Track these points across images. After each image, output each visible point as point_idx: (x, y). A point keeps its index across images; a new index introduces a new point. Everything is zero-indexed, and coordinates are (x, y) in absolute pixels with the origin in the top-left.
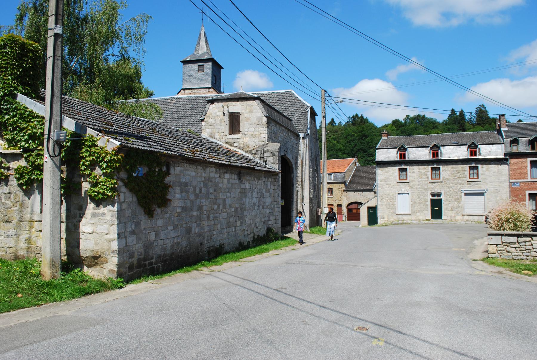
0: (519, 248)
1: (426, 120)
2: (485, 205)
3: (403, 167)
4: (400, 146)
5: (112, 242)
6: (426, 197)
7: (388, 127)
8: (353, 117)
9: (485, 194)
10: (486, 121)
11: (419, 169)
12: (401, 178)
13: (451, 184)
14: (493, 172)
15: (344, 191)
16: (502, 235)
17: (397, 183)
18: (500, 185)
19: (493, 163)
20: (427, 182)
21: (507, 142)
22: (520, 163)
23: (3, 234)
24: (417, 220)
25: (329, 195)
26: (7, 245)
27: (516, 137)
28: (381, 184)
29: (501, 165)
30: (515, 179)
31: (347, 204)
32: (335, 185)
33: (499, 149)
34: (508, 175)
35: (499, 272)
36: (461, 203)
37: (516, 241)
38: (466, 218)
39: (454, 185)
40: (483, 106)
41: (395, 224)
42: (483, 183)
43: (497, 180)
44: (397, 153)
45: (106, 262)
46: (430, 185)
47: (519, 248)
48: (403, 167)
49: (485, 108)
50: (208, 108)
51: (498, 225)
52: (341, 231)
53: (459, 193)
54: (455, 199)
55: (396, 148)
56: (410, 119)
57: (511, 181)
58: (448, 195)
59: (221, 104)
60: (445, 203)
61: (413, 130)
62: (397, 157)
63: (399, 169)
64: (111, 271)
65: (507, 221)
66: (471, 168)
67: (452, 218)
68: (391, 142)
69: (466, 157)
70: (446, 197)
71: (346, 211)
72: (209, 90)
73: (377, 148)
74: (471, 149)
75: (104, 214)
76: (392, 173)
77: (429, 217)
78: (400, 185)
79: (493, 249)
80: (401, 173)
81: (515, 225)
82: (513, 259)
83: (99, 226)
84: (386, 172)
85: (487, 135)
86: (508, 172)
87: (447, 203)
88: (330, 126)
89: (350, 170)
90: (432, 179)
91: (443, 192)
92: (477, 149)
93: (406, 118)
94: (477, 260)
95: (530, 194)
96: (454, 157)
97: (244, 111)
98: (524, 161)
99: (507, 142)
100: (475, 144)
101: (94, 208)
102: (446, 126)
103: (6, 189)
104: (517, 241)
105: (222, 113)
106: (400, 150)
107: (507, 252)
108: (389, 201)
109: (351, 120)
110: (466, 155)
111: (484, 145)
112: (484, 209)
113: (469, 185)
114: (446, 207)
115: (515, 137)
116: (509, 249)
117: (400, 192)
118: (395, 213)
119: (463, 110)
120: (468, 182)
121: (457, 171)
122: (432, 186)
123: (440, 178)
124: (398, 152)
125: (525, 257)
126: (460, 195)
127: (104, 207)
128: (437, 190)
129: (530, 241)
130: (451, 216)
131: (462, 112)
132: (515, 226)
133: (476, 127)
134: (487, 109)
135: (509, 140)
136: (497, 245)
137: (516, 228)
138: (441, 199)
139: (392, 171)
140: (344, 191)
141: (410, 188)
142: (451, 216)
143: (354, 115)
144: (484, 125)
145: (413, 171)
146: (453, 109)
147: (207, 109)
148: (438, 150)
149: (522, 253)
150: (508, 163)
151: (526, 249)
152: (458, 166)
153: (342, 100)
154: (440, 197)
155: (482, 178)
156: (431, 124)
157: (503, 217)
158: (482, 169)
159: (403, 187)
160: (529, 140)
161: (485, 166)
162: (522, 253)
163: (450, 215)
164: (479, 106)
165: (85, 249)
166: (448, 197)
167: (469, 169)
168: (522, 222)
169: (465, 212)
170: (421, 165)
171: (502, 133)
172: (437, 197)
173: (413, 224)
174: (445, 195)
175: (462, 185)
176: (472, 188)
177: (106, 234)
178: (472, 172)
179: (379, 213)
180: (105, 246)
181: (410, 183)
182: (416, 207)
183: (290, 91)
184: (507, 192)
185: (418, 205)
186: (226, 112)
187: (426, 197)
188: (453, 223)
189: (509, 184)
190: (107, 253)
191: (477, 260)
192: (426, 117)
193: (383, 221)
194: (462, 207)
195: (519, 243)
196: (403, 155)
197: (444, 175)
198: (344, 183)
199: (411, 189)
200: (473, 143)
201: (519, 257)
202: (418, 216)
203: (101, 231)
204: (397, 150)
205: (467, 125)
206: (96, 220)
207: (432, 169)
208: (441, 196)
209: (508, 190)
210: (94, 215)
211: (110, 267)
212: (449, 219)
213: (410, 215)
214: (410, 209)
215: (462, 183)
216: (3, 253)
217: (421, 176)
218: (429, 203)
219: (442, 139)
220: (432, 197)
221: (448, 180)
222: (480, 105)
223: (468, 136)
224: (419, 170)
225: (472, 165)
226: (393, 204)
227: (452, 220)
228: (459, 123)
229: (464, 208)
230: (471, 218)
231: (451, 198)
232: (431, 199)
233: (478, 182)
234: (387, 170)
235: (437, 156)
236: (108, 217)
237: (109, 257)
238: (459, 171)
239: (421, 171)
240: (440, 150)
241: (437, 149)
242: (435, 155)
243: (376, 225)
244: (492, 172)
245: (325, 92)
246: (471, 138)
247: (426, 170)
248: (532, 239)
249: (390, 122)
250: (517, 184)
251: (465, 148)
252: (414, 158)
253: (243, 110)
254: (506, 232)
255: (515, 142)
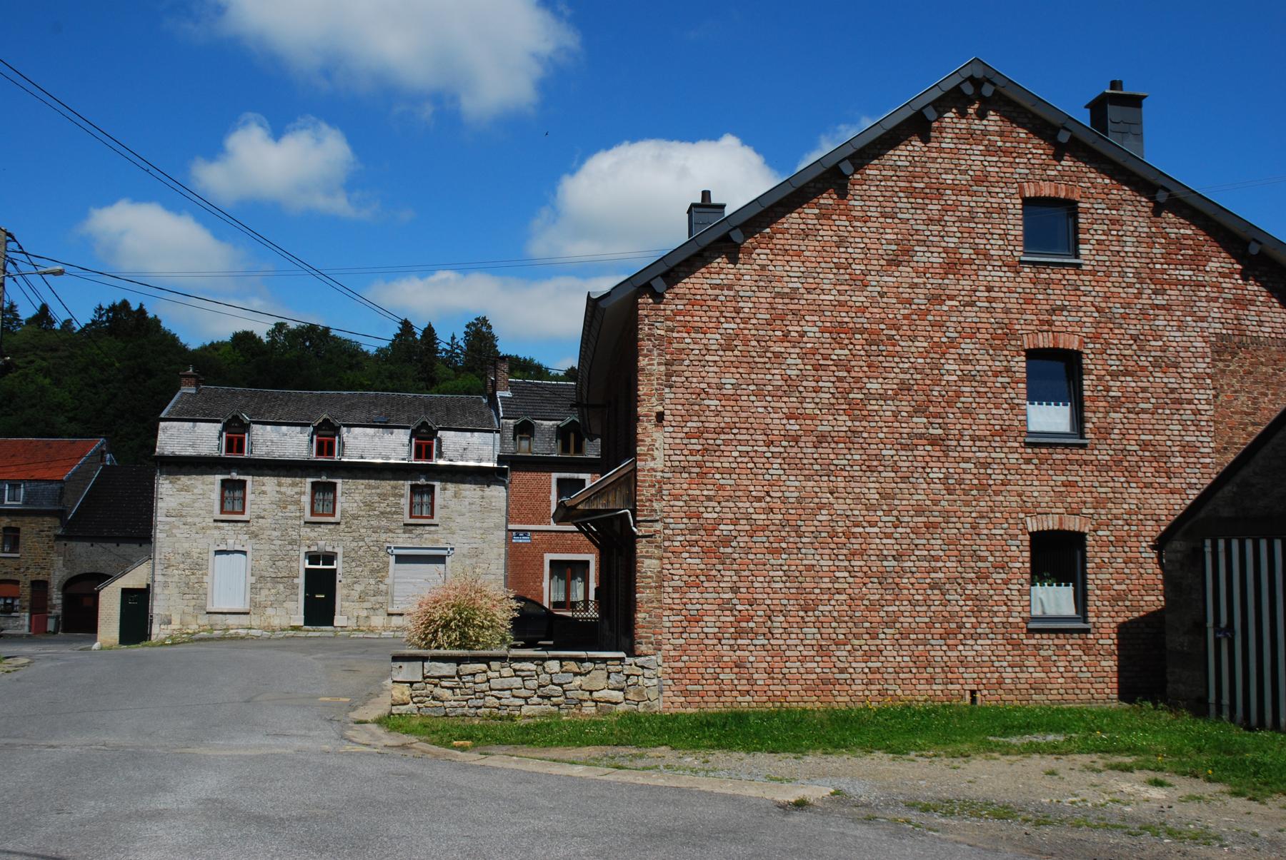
0: (460, 688)
1: (332, 343)
6: (294, 564)
7: (220, 352)
8: (113, 308)
9: (448, 559)
11: (280, 485)
13: (363, 531)
15: (58, 537)
16: (424, 659)
22: (534, 482)
24: (264, 629)
25: (7, 549)
27: (528, 418)
28: (167, 523)
29: (488, 486)
30: (521, 522)
31: (66, 579)
32: (27, 519)
33: (486, 444)
34: (504, 513)
35: (404, 747)
36: (387, 581)
37: (453, 673)
39: (370, 532)
40: (484, 321)
41: (201, 640)
42: (444, 529)
43: (478, 525)
44: (221, 435)
46: (306, 531)
47: (460, 688)
49: (490, 327)
51: (427, 635)
52: (26, 661)
54: (372, 571)
55: (218, 422)
57: (511, 527)
60: (344, 581)
62: (219, 448)
65: (446, 626)
66: (415, 490)
68: (206, 402)
69: (404, 459)
71: (59, 601)
73: (162, 415)
77: (299, 620)
78: (222, 528)
79: (403, 694)
80: (227, 494)
81: (464, 635)
82: (446, 715)
84: (186, 489)
85: (463, 405)
88: (34, 328)
89: (82, 475)
91: (339, 551)
93: (273, 331)
94: (366, 722)
95: (552, 562)
96: (373, 458)
102: (385, 367)
104: (457, 672)
107: (434, 698)
109: (104, 319)
110: (405, 455)
111: (453, 433)
113: (407, 535)
114: (345, 592)
116: (438, 691)
117: (223, 547)
118: (203, 607)
120: (405, 525)
121: (379, 495)
122: (312, 535)
123: (333, 514)
124: (224, 434)
125: (473, 711)
126: (385, 559)
128: (325, 545)
129: (485, 672)
132: (465, 637)
133: (462, 375)
134: (495, 331)
136: (412, 683)
137: (464, 642)
138: (335, 570)
139: (201, 486)
140: (58, 537)
143: (117, 304)
149: (467, 701)
150: (507, 482)
151: (475, 692)
153: (59, 267)
157: (437, 616)
158: (444, 493)
159: (231, 533)
160: (558, 426)
162: (467, 701)
163: (355, 614)
168: (482, 627)
173: (253, 638)
175: (391, 535)
178: (417, 499)
182: (265, 592)
185: (269, 585)
187: (294, 564)
188: (361, 635)
191: (366, 722)
193: (168, 632)
195: (460, 677)
196: (235, 443)
197: (346, 505)
198: (60, 514)
199: (253, 541)
200: (424, 424)
201: (459, 711)
204: (219, 426)
205: (441, 369)
207: (315, 486)
212: (352, 624)
213: (248, 613)
217: (282, 504)
218: (301, 581)
219: (347, 406)
221: (355, 517)
223: (417, 403)
224: (278, 489)
226: (200, 582)
229: (392, 597)
231: (360, 569)
233: (433, 528)
234: (189, 483)
239: (283, 489)
241: (332, 433)
242: (325, 447)
243: (144, 643)
245: (8, 238)
246: (423, 409)
247: (297, 489)
248: (489, 667)
249: (227, 338)
251: (402, 436)
252: (267, 454)
254: (442, 652)
255: (525, 430)
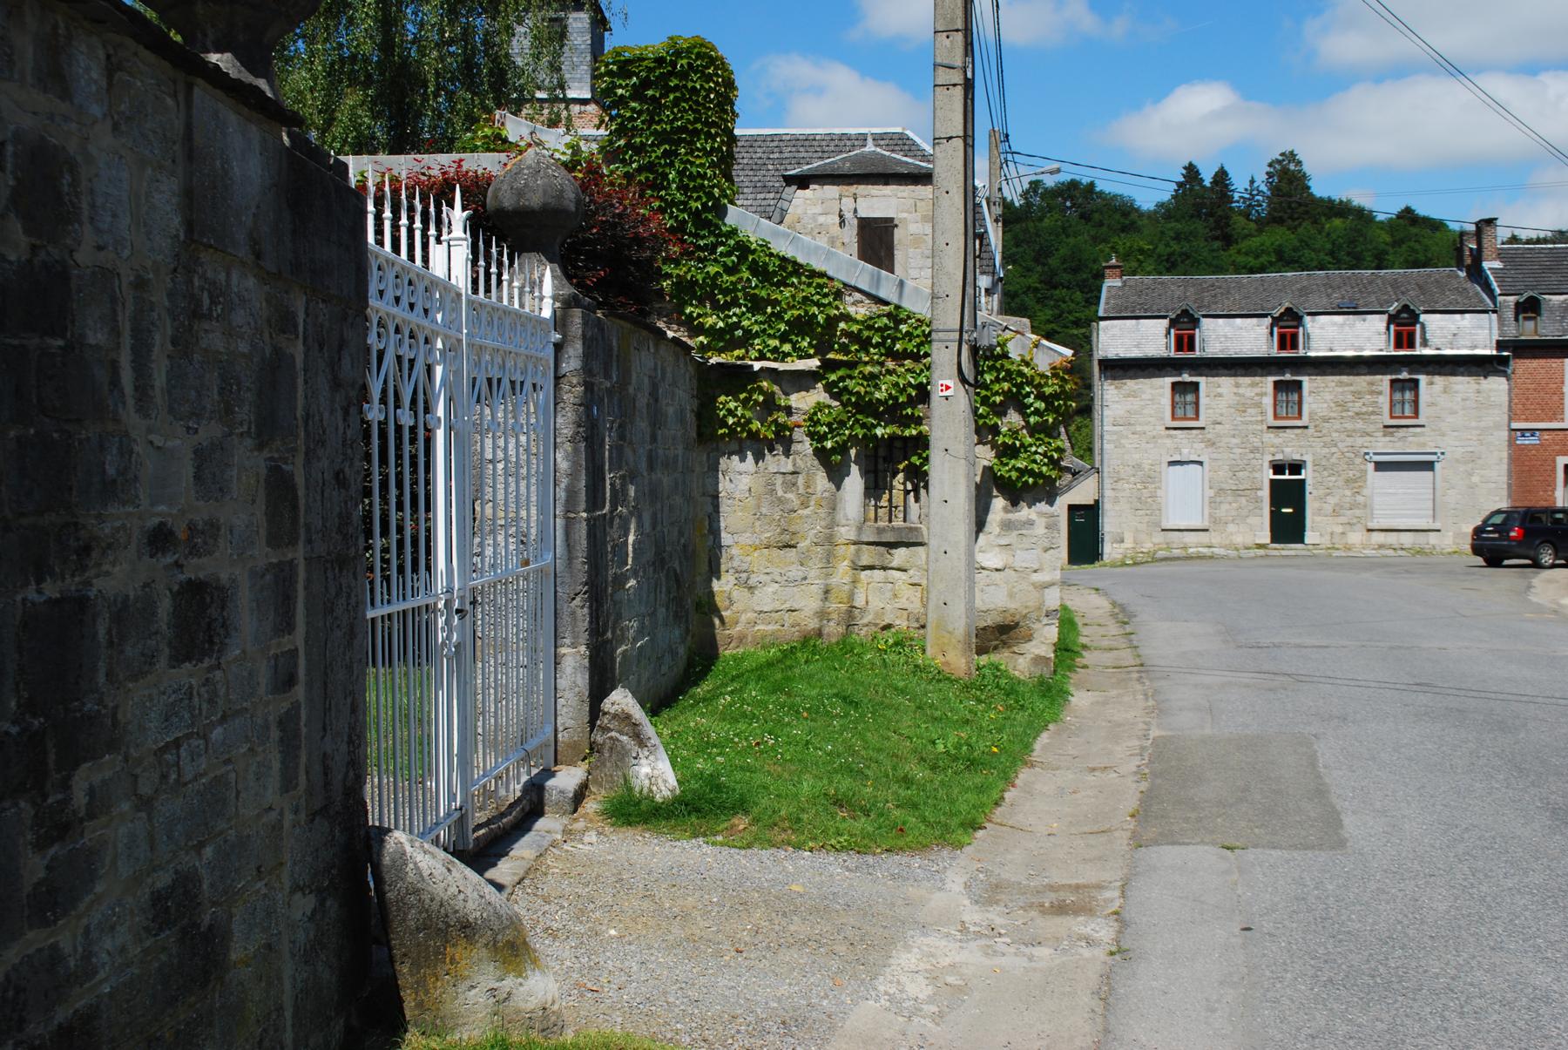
2: (1434, 500)
3: (1186, 378)
4: (1179, 312)
5: (1046, 590)
9: (1437, 466)
10: (1301, 209)
11: (1237, 385)
12: (1179, 412)
14: (1463, 400)
17: (1167, 428)
18: (1481, 437)
19: (1462, 369)
20: (1259, 428)
21: (1506, 307)
22: (1543, 371)
23: (778, 578)
24: (1226, 547)
26: (787, 606)
28: (1115, 433)
29: (1485, 377)
30: (1527, 420)
33: (1481, 328)
34: (1506, 409)
36: (1365, 492)
38: (1378, 538)
39: (1343, 436)
42: (1434, 430)
43: (1474, 424)
44: (1168, 333)
45: (1029, 638)
46: (1270, 437)
48: (1186, 378)
49: (1299, 163)
50: (790, 202)
53: (1358, 460)
54: (1347, 481)
56: (1043, 197)
57: (1515, 425)
58: (1325, 470)
59: (831, 191)
60: (1315, 492)
61: (1057, 236)
63: (1174, 385)
64: (1038, 660)
67: (1334, 541)
69: (1381, 350)
70: (1317, 474)
72: (583, 108)
74: (1397, 325)
75: (1031, 523)
76: (1150, 397)
77: (1265, 536)
80: (1177, 398)
83: (1018, 552)
84: (1133, 395)
86: (1505, 399)
87: (1322, 492)
90: (1276, 417)
91: (1308, 458)
92: (1418, 327)
97: (905, 215)
98: (1554, 365)
99: (1506, 307)
100: (1413, 311)
101: (1006, 510)
103: (787, 465)
105: (837, 220)
106: (1179, 323)
108: (1139, 486)
110: (1382, 345)
112: (1431, 512)
113: (1388, 439)
114: (1317, 505)
115: (1531, 293)
117: (1177, 458)
118: (1158, 524)
119: (1226, 168)
120: (1386, 427)
121: (1353, 393)
122: (1277, 441)
124: (1172, 331)
126: (1362, 467)
127: (1030, 507)
128: (1291, 454)
130: (1332, 534)
131: (1221, 177)
134: (1306, 168)
135: (1512, 299)
138: (1303, 482)
141: (1206, 447)
142: (1332, 534)
144: (1296, 223)
145: (1217, 392)
146: (1191, 164)
147: (785, 205)
148: (1297, 327)
150: (1509, 371)
152: (1356, 378)
153: (1055, 165)
154: (1300, 474)
155: (1427, 418)
156: (1117, 216)
158: (1431, 388)
161: (1439, 381)
163: (1329, 530)
164: (1280, 158)
165: (985, 609)
166: (1326, 473)
167: (1391, 387)
169: (1375, 520)
170: (1243, 372)
171: (1487, 278)
172: (1290, 474)
174: (1316, 468)
175: (1368, 438)
176: (1399, 447)
177: (1035, 571)
179: (1105, 525)
180: (1032, 599)
181: (1206, 431)
182: (1225, 507)
183: (899, 130)
184: (1501, 459)
185: (1230, 499)
186: (849, 215)
189: (1510, 436)
190: (1034, 615)
192: (1098, 189)
193: (1121, 551)
194: (1365, 506)
196: (1186, 340)
197: (1314, 406)
199: (1210, 450)
202: (1232, 534)
203: (1024, 565)
204: (1165, 322)
206: (1012, 538)
208: (1303, 471)
209: (1505, 455)
210: (1007, 526)
211: (1037, 652)
212: (1325, 541)
213: (1207, 530)
214: (1206, 512)
215: (1368, 430)
216: (777, 627)
218: (1265, 493)
220: (1275, 474)
221: (1326, 420)
222: (1282, 154)
224: (1235, 390)
225: (1400, 377)
227: (1336, 546)
228: (1211, 214)
229: (1372, 510)
230: (1392, 538)
231: (1333, 479)
232: (1272, 482)
233: (1418, 430)
234: (1136, 387)
235: (1294, 346)
236: (1040, 529)
237: (1036, 626)
238: (1359, 393)
239: (1241, 391)
240: (1303, 326)
241: (1294, 323)
242: (1288, 341)
243: (1097, 564)
244: (1459, 399)
247: (1257, 390)
250: (1532, 436)
251: (1378, 323)
253: (902, 212)
255: (1529, 308)
